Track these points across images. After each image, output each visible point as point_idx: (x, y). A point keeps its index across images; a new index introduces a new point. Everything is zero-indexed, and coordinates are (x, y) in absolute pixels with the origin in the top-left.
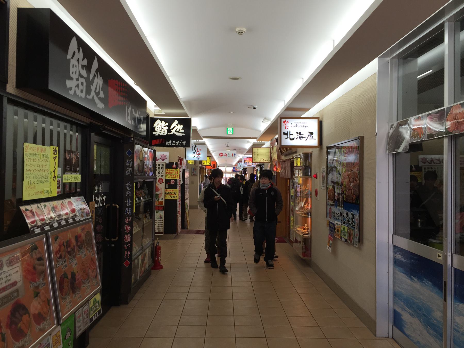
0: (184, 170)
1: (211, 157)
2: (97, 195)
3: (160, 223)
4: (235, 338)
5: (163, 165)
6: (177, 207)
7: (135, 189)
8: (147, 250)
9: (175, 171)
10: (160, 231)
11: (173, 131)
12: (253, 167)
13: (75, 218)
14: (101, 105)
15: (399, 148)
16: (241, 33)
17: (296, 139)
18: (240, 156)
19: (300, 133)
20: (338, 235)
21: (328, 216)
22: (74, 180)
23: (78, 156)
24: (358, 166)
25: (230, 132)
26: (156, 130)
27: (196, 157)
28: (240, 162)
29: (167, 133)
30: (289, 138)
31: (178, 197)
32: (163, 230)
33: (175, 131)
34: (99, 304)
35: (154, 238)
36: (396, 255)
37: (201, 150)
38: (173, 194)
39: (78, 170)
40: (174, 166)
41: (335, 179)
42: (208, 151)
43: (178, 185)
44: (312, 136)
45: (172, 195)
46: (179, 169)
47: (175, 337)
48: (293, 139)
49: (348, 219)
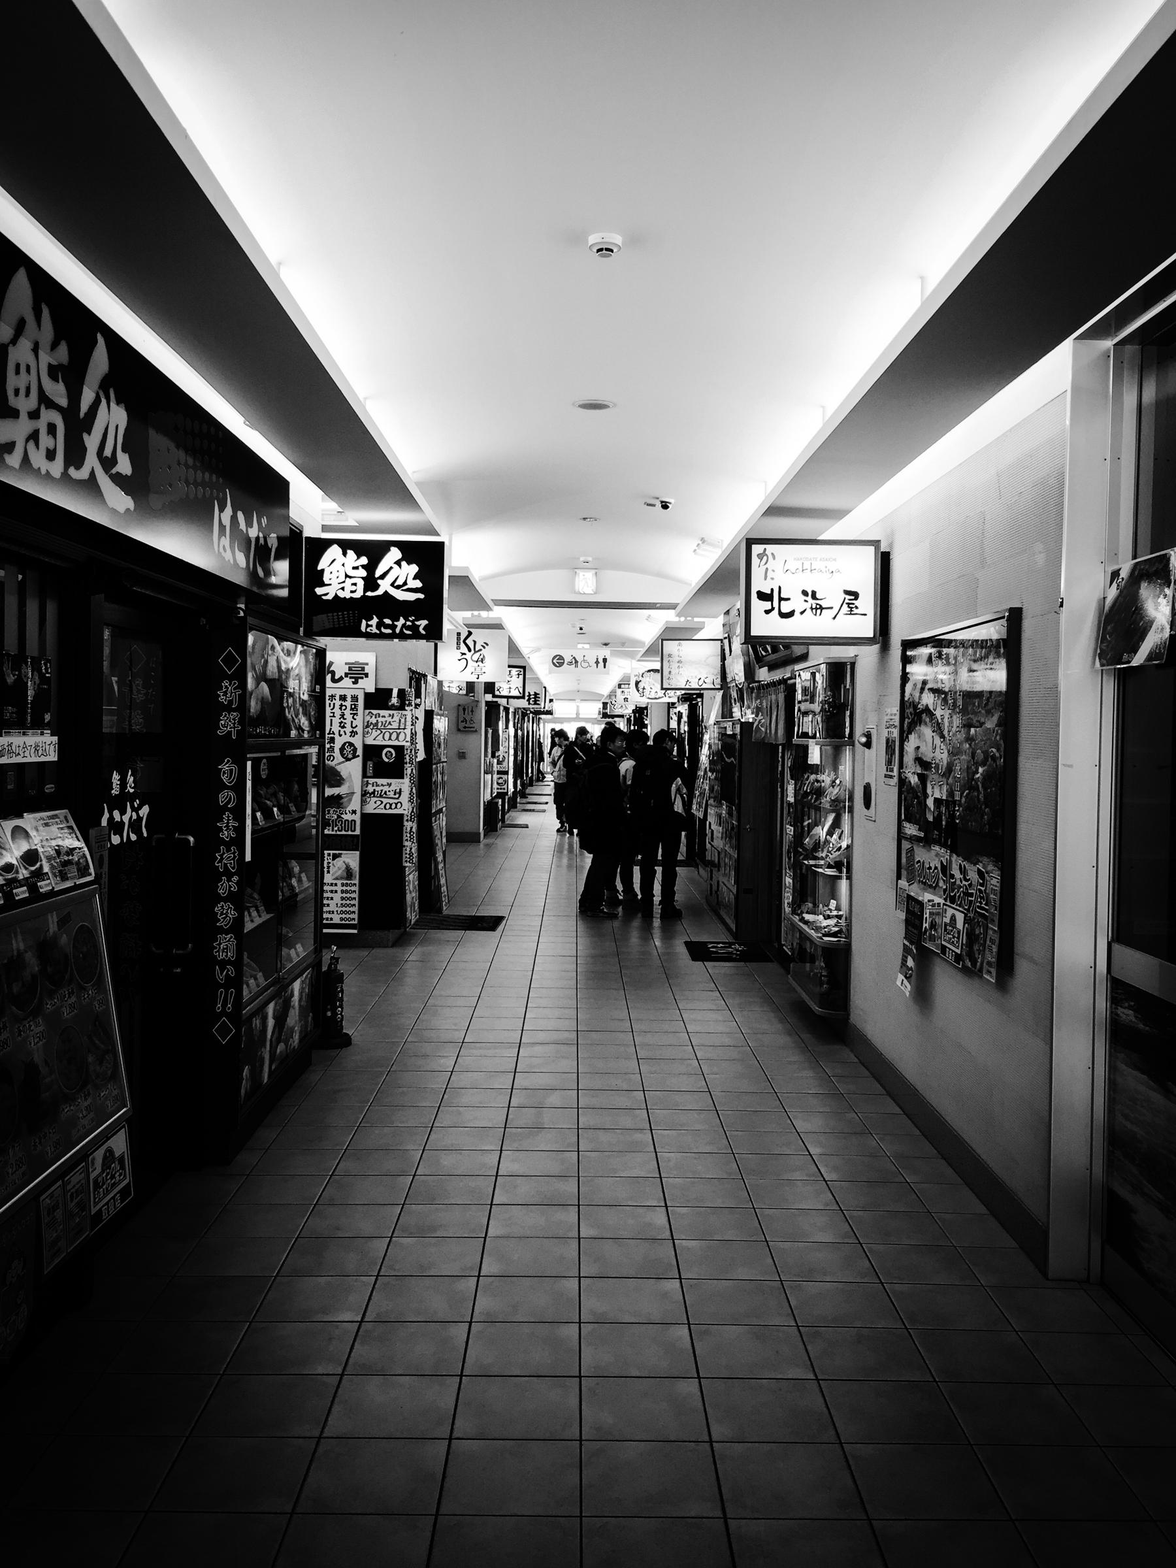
0: (429, 715)
1: (524, 668)
2: (119, 803)
3: (347, 892)
4: (580, 1277)
5: (355, 698)
6: (405, 838)
7: (249, 784)
8: (297, 985)
9: (396, 718)
10: (347, 919)
11: (384, 586)
12: (669, 703)
13: (39, 884)
14: (119, 500)
15: (1135, 650)
16: (604, 252)
17: (802, 613)
18: (621, 667)
19: (814, 594)
20: (932, 938)
21: (904, 873)
22: (33, 755)
23: (47, 675)
24: (1001, 709)
25: (585, 585)
26: (326, 580)
27: (470, 669)
28: (623, 686)
29: (365, 591)
30: (776, 612)
31: (405, 807)
32: (356, 916)
33: (392, 585)
34: (123, 1167)
35: (322, 942)
36: (1120, 1010)
37: (487, 645)
38: (391, 794)
39: (46, 721)
40: (394, 700)
41: (927, 754)
42: (513, 649)
43: (408, 765)
44: (853, 604)
45: (385, 801)
46: (412, 710)
47: (378, 1276)
48: (790, 614)
49: (966, 889)
